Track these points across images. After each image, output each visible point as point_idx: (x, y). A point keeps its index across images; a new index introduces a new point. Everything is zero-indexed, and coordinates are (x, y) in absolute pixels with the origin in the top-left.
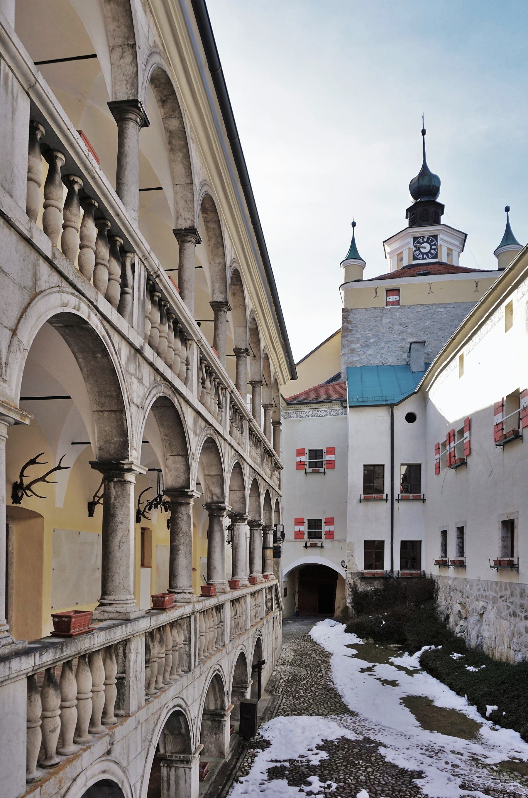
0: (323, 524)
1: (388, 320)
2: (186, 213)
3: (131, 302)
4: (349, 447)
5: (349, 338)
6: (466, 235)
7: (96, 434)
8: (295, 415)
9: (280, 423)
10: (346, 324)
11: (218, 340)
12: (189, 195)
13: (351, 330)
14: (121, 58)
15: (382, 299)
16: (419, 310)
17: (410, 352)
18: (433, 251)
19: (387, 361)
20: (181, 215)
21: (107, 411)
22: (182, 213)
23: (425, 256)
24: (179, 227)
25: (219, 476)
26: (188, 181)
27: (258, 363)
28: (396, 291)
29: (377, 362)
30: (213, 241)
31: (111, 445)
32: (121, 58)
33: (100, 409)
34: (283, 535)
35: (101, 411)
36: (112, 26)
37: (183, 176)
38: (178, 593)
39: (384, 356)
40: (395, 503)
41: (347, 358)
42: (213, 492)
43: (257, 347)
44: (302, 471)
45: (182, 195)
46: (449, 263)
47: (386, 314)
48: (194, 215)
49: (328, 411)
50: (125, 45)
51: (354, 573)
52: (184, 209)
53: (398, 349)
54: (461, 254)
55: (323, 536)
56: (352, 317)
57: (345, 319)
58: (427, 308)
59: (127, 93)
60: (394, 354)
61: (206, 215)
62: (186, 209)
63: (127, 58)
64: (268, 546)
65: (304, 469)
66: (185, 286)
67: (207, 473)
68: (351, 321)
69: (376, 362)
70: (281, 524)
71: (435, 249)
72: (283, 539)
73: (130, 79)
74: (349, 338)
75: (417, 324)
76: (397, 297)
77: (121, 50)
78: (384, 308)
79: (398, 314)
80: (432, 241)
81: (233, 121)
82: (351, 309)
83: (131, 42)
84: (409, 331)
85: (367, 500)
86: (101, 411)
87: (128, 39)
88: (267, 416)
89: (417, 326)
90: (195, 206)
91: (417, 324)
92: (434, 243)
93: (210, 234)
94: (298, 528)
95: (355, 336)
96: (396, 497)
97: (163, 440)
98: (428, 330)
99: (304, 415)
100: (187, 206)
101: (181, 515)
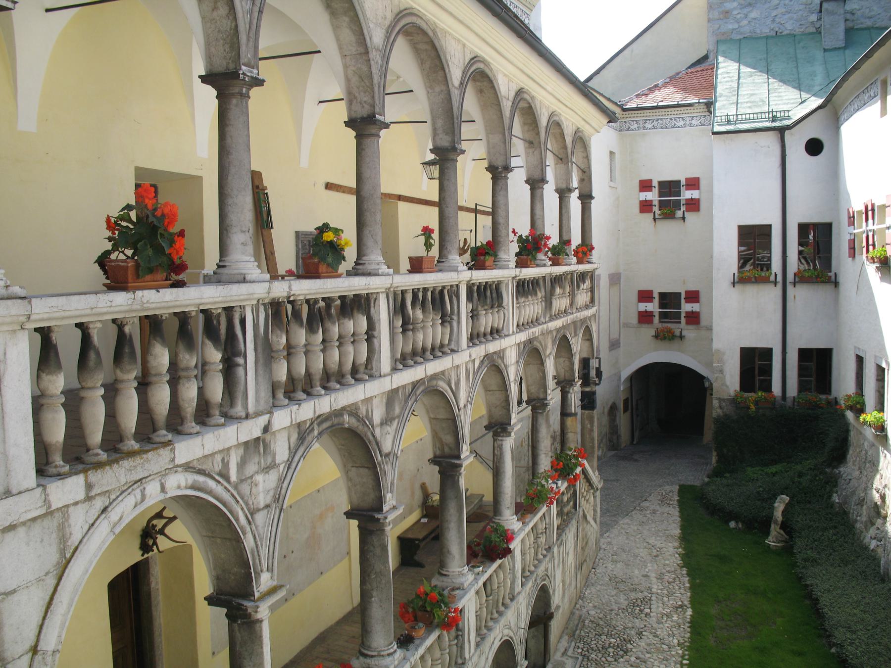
0: (683, 301)
2: (362, 93)
3: (243, 378)
4: (715, 197)
7: (211, 562)
8: (636, 126)
9: (591, 197)
12: (365, 68)
14: (213, 10)
17: (821, 11)
19: (782, 27)
20: (355, 98)
21: (220, 538)
22: (357, 95)
25: (450, 421)
30: (427, 65)
31: (231, 575)
32: (213, 10)
33: (210, 535)
34: (599, 373)
35: (213, 537)
37: (354, 45)
38: (372, 656)
40: (790, 288)
42: (444, 441)
43: (533, 129)
48: (373, 97)
51: (723, 400)
52: (358, 88)
53: (801, 7)
55: (683, 320)
59: (225, 58)
60: (795, 16)
61: (412, 38)
62: (361, 88)
64: (568, 411)
65: (652, 212)
66: (365, 207)
67: (432, 416)
72: (600, 379)
73: (228, 37)
86: (213, 537)
93: (422, 56)
94: (643, 307)
96: (790, 277)
97: (339, 450)
101: (372, 548)
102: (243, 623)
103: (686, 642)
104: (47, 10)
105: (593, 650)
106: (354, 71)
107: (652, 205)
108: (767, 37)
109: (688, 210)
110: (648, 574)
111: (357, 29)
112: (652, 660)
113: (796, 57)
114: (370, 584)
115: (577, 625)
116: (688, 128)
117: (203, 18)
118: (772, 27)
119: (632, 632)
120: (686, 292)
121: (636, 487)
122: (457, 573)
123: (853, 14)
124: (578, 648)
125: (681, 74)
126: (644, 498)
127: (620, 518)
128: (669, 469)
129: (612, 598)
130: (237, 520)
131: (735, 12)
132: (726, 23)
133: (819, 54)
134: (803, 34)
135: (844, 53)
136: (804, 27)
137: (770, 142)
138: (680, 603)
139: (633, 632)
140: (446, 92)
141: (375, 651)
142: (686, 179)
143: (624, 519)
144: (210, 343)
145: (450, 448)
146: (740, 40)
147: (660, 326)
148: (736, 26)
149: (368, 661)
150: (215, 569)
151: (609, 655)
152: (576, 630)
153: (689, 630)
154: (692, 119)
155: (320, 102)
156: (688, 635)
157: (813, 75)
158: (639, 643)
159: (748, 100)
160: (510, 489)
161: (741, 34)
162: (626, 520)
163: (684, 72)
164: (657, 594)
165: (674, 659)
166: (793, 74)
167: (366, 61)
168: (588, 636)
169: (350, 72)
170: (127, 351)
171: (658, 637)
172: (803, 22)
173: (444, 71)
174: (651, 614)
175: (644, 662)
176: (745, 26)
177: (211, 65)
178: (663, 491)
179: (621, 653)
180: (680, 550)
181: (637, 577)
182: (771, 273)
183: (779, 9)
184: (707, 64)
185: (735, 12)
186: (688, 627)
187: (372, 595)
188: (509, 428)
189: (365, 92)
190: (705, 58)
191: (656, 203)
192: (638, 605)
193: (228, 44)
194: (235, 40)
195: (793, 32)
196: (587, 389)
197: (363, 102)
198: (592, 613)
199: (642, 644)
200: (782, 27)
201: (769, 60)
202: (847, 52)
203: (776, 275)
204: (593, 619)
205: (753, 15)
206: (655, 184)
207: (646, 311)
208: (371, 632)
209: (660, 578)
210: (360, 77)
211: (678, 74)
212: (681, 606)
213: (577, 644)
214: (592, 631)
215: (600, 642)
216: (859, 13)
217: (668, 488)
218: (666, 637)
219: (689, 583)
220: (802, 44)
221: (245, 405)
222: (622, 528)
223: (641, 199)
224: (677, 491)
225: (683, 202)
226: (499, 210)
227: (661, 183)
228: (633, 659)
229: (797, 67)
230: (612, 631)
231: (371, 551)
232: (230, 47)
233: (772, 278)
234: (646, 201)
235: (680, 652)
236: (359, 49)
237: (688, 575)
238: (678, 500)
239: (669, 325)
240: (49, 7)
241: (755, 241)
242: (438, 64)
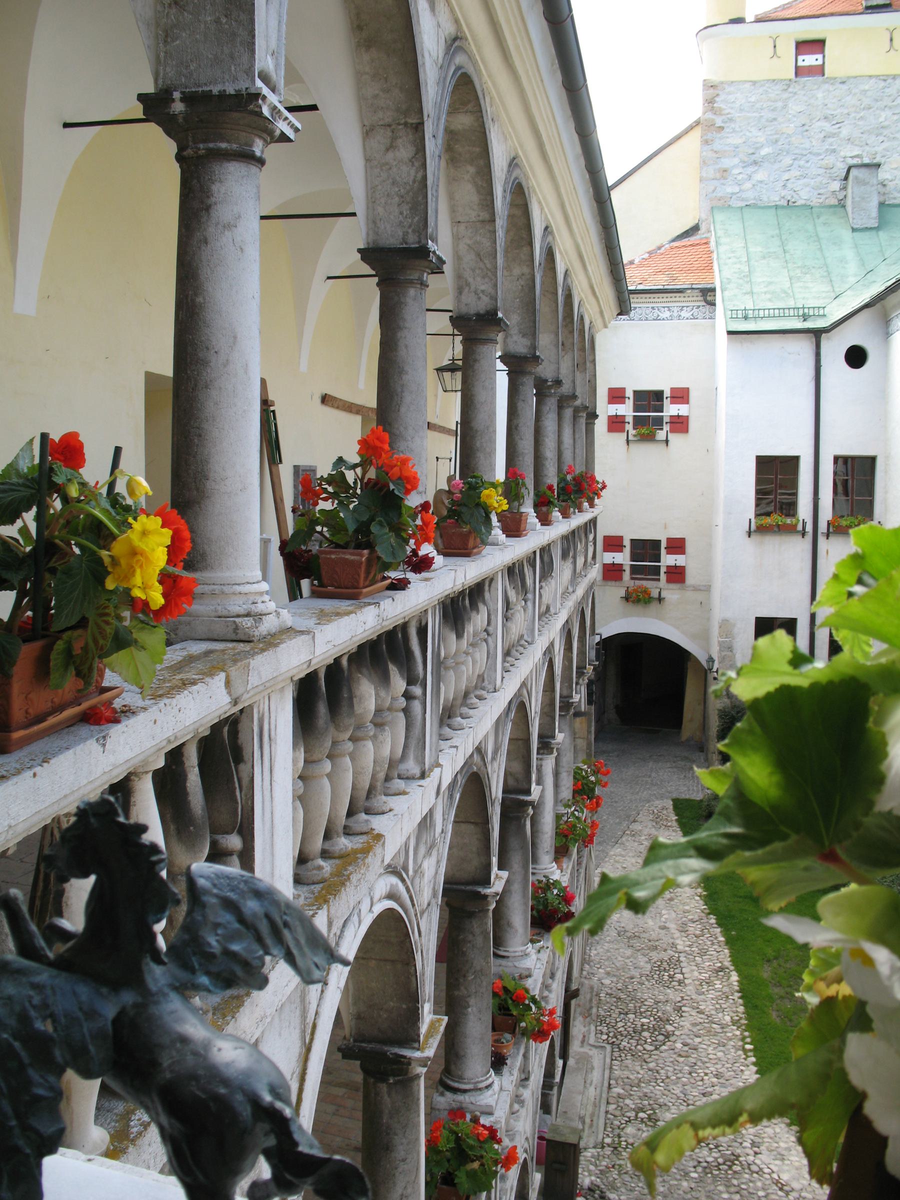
0: (663, 551)
1: (799, 108)
2: (479, 279)
3: (419, 717)
5: (717, 146)
7: (350, 994)
11: (517, 438)
12: (487, 243)
16: (867, 88)
17: (846, 178)
19: (795, 196)
20: (468, 285)
21: (376, 959)
22: (470, 280)
24: (464, 310)
25: (520, 742)
26: (485, 215)
28: (817, 45)
29: (777, 199)
32: (387, 150)
37: (475, 207)
38: (465, 1091)
40: (821, 540)
41: (712, 188)
45: (469, 242)
47: (795, 93)
48: (496, 285)
49: (675, 309)
50: (399, 124)
52: (473, 270)
53: (822, 171)
55: (663, 577)
58: (883, 84)
60: (812, 182)
62: (477, 271)
63: (402, 150)
68: (720, 109)
73: (408, 193)
74: (717, 146)
75: (862, 118)
77: (389, 134)
79: (820, 95)
81: (581, 75)
82: (722, 83)
83: (413, 120)
84: (845, 132)
85: (762, 530)
87: (406, 113)
88: (577, 430)
89: (861, 123)
90: (498, 249)
91: (862, 118)
94: (610, 558)
95: (729, 141)
96: (823, 527)
98: (885, 132)
100: (482, 265)
101: (470, 937)
102: (396, 1083)
103: (741, 1018)
104: (66, 125)
105: (622, 1035)
106: (469, 245)
107: (624, 422)
108: (777, 207)
109: (673, 430)
110: (667, 925)
111: (485, 185)
112: (705, 1047)
113: (817, 235)
114: (466, 988)
115: (591, 1000)
116: (676, 322)
117: (368, 160)
118: (783, 195)
119: (668, 1008)
120: (668, 539)
121: (616, 802)
122: (520, 954)
123: (884, 185)
124: (602, 1033)
125: (663, 249)
126: (632, 819)
127: (609, 847)
128: (650, 776)
129: (627, 961)
130: (413, 933)
131: (736, 171)
132: (724, 184)
133: (847, 235)
134: (823, 206)
135: (878, 236)
136: (823, 197)
137: (803, 348)
138: (719, 965)
139: (669, 1008)
140: (528, 277)
141: (469, 1083)
142: (672, 389)
143: (614, 849)
144: (396, 669)
145: (517, 780)
146: (742, 208)
147: (632, 583)
148: (737, 189)
149: (460, 1097)
150: (355, 1004)
151: (646, 1041)
152: (591, 1008)
153: (741, 1001)
154: (682, 310)
155: (329, 278)
156: (741, 1009)
157: (843, 260)
158: (681, 1023)
159: (765, 290)
160: (551, 826)
161: (743, 200)
162: (618, 850)
163: (667, 246)
164: (685, 952)
165: (732, 1043)
166: (817, 259)
167: (490, 231)
168: (610, 1016)
169: (462, 247)
170: (345, 696)
171: (703, 1013)
172: (822, 191)
173: (532, 246)
174: (686, 981)
175: (695, 1049)
176: (748, 190)
177: (377, 233)
178: (652, 808)
179: (661, 1038)
180: (700, 890)
181: (654, 930)
182: (798, 520)
183: (791, 172)
184: (698, 237)
185: (736, 171)
186: (740, 998)
187: (468, 1003)
188: (553, 742)
189: (483, 277)
190: (695, 229)
191: (630, 419)
192: (665, 969)
193: (408, 203)
194: (420, 199)
195: (808, 203)
197: (479, 292)
198: (607, 982)
199: (686, 1024)
200: (795, 196)
201: (784, 237)
202: (881, 233)
203: (804, 523)
204: (609, 991)
206: (629, 394)
207: (613, 564)
208: (464, 1056)
209: (683, 929)
210: (478, 255)
211: (659, 248)
212: (721, 969)
213: (599, 1028)
214: (613, 1008)
215: (629, 1024)
216: (891, 185)
217: (659, 803)
218: (713, 1012)
219: (723, 936)
220: (822, 219)
221: (420, 758)
222: (616, 862)
223: (610, 414)
224: (671, 807)
225: (666, 420)
226: (547, 440)
227: (637, 393)
228: (679, 1045)
229: (821, 249)
230: (640, 1007)
231: (470, 942)
232: (411, 209)
233: (800, 527)
234: (616, 416)
235: (738, 1033)
236: (482, 214)
237: (720, 924)
238: (676, 820)
239: (644, 583)
240: (70, 120)
241: (776, 477)
242: (524, 236)
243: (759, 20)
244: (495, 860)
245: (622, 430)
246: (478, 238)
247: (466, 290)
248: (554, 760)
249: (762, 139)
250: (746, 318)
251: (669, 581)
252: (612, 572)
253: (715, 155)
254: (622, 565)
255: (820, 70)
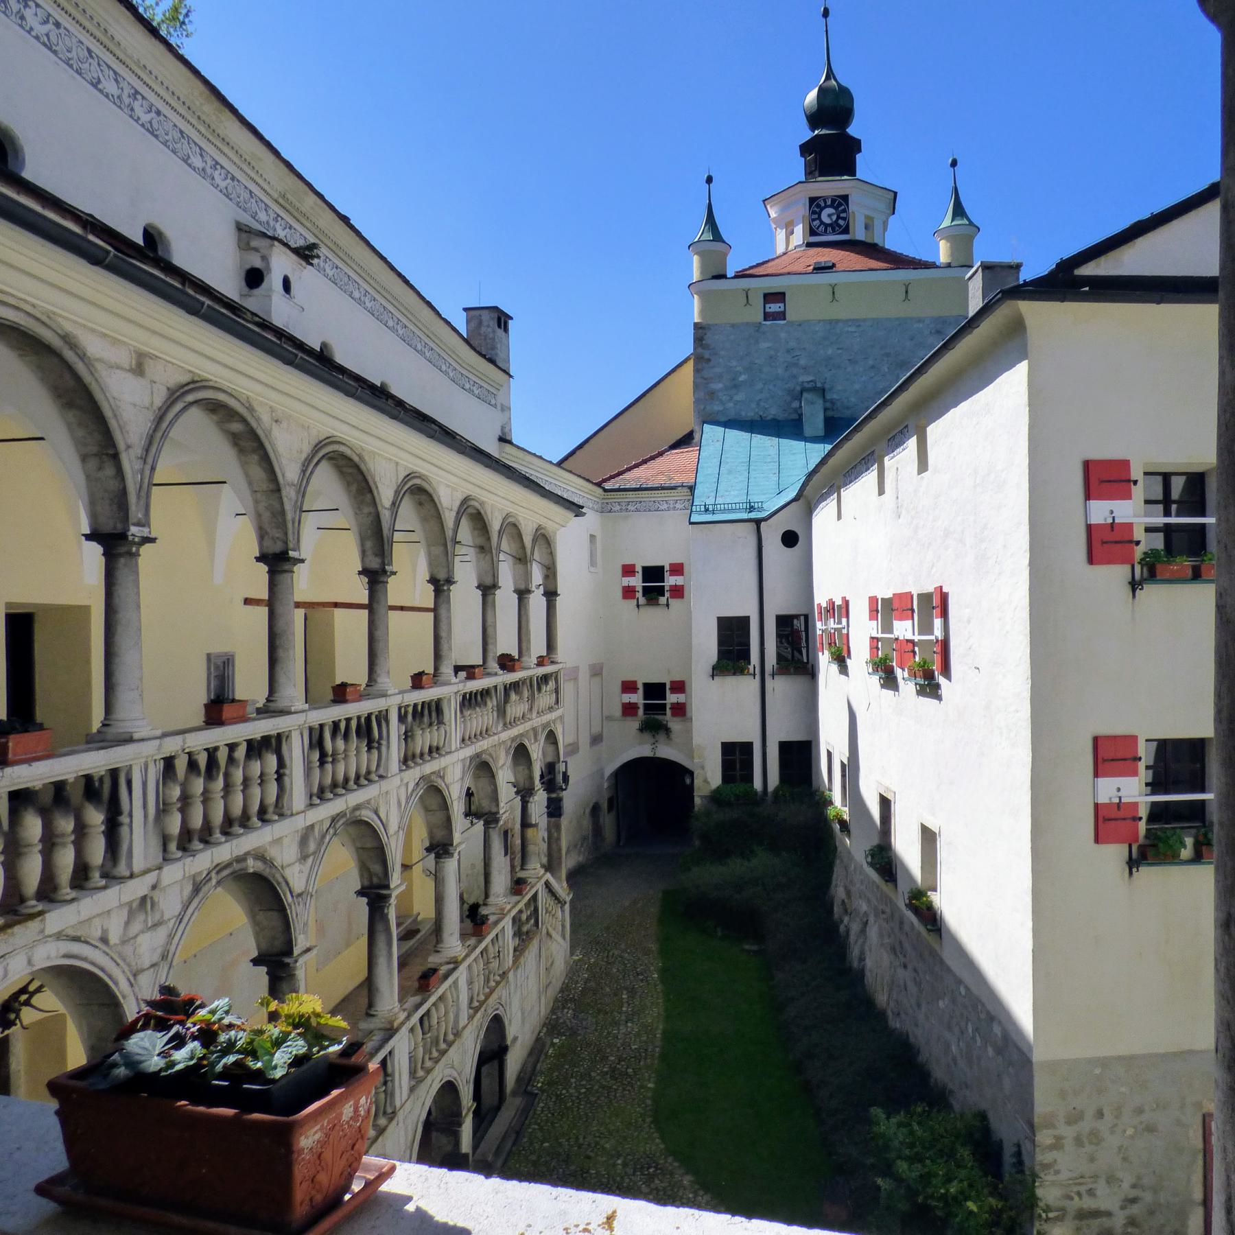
0: (668, 692)
1: (770, 345)
6: (895, 193)
10: (700, 350)
13: (709, 360)
15: (755, 313)
18: (841, 222)
20: (267, 533)
22: (269, 530)
23: (829, 229)
26: (272, 487)
27: (488, 557)
28: (779, 297)
30: (354, 488)
36: (80, 433)
39: (762, 404)
44: (632, 600)
46: (869, 240)
54: (892, 219)
55: (668, 711)
56: (710, 338)
57: (699, 340)
69: (749, 414)
70: (562, 759)
71: (844, 219)
76: (782, 305)
78: (760, 323)
80: (840, 205)
83: (111, 452)
88: (522, 608)
92: (843, 207)
99: (633, 508)
109: (672, 596)
155: (237, 515)
169: (261, 507)
191: (640, 589)
196: (554, 795)
205: (738, 397)
206: (639, 569)
225: (667, 588)
243: (736, 277)
244: (418, 936)
245: (633, 597)
246: (271, 502)
247: (266, 537)
248: (456, 863)
249: (739, 369)
250: (707, 510)
251: (674, 714)
252: (629, 709)
253: (705, 381)
254: (636, 704)
255: (781, 315)
